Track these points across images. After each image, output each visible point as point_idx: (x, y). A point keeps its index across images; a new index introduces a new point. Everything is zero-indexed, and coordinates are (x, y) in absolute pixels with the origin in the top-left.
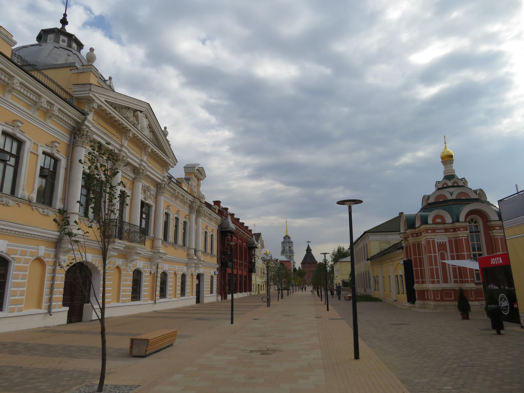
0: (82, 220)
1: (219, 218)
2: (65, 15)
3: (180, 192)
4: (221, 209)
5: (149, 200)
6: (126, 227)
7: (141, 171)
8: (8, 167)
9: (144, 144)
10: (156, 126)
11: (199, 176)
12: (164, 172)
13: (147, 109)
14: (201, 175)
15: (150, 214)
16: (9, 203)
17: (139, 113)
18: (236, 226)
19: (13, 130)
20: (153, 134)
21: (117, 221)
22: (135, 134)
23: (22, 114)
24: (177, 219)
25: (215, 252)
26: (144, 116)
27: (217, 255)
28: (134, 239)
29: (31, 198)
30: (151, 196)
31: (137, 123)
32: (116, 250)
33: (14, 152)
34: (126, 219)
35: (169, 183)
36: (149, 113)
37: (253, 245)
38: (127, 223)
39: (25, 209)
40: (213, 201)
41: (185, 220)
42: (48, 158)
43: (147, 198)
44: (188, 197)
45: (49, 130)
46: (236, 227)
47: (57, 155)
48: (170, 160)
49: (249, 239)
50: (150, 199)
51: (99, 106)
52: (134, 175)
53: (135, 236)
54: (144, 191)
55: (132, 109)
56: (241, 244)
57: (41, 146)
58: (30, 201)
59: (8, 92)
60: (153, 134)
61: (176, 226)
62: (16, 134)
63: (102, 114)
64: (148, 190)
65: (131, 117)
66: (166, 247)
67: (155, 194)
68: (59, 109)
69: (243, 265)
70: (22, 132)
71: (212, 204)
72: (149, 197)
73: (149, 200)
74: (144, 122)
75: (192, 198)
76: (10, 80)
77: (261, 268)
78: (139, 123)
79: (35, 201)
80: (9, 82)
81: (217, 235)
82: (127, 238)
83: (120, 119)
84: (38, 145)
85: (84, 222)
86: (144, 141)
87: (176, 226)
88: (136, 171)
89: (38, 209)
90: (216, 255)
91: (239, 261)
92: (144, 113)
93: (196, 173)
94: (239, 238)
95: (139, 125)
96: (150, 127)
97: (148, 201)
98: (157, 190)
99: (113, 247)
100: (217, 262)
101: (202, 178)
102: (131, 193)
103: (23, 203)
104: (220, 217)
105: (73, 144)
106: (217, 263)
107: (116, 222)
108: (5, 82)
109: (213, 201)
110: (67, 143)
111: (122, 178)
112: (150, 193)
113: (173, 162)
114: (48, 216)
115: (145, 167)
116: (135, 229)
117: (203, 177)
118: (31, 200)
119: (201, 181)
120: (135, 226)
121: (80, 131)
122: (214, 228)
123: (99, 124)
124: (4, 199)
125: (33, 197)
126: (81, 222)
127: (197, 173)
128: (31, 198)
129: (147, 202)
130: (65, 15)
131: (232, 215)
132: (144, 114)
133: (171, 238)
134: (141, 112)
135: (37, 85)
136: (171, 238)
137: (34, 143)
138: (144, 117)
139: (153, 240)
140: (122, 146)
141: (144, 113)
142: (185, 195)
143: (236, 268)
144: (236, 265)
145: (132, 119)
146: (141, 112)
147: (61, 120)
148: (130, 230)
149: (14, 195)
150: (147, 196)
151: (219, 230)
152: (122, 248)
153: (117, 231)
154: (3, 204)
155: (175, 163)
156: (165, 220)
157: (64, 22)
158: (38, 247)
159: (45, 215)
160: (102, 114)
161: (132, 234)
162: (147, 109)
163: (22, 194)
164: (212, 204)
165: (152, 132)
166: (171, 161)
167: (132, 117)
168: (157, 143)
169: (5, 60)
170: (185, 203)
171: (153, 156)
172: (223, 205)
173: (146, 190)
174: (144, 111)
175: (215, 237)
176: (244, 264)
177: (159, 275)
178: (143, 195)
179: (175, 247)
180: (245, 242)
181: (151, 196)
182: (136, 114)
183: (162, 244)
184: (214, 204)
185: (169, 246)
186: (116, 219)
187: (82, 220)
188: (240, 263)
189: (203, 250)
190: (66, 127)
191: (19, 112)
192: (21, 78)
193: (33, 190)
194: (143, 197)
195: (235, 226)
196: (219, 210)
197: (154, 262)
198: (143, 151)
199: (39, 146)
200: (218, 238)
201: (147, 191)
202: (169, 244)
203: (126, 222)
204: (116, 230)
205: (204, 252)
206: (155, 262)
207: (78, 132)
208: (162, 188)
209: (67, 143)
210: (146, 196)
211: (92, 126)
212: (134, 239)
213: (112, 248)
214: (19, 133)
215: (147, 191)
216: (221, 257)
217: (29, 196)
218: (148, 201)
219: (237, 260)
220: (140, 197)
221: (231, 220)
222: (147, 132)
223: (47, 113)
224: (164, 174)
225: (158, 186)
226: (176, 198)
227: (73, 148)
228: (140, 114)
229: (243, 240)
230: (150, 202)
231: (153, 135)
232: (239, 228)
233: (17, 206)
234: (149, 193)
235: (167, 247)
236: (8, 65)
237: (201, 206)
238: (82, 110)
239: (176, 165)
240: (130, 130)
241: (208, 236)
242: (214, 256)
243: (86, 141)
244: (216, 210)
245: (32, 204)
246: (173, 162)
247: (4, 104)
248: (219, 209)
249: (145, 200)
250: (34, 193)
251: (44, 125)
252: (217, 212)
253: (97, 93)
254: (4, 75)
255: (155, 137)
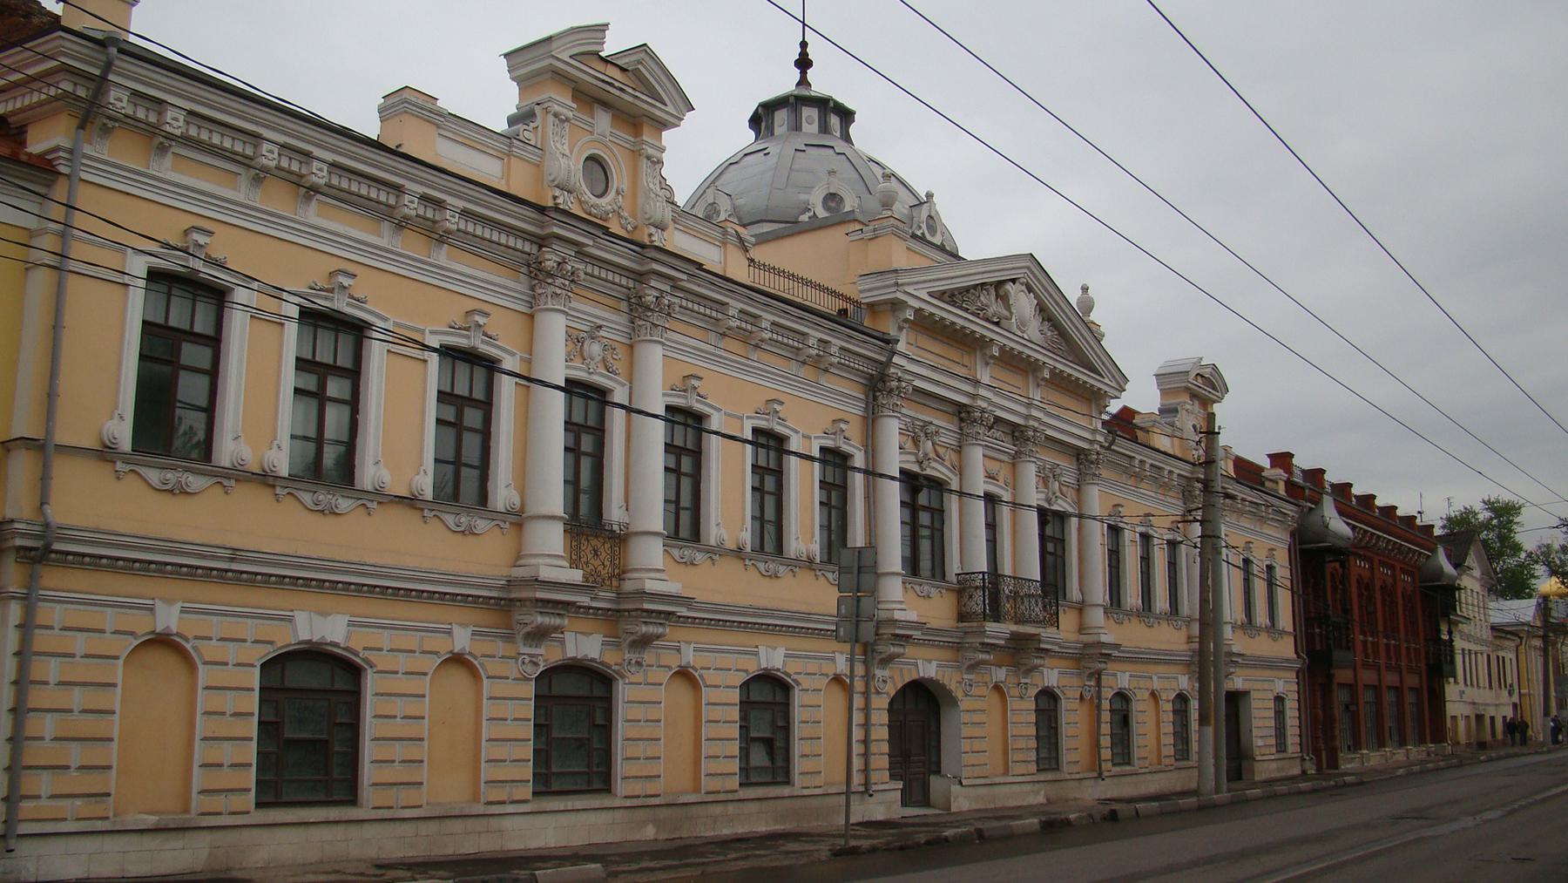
0: (747, 561)
1: (1289, 509)
2: (804, 45)
3: (1145, 459)
4: (1298, 479)
5: (1060, 501)
6: (1006, 590)
7: (1031, 433)
8: (467, 436)
9: (1093, 392)
10: (1058, 304)
11: (1207, 393)
12: (978, 367)
13: (1028, 268)
14: (1213, 389)
15: (1066, 537)
16: (337, 507)
17: (1009, 286)
18: (1350, 521)
19: (834, 440)
20: (1052, 326)
21: (984, 576)
22: (921, 310)
23: (355, 251)
24: (1146, 538)
25: (1285, 619)
26: (1024, 288)
27: (1295, 630)
28: (1030, 615)
29: (269, 466)
30: (1064, 489)
31: (1007, 314)
32: (989, 647)
33: (479, 394)
34: (1007, 568)
35: (1112, 443)
36: (1035, 276)
37: (1438, 581)
38: (1009, 577)
39: (805, 576)
40: (1269, 456)
41: (1268, 563)
42: (463, 370)
43: (1054, 499)
44: (1172, 469)
45: (199, 203)
46: (1354, 528)
47: (845, 448)
48: (1106, 381)
49: (1422, 560)
50: (1062, 499)
51: (918, 311)
52: (1014, 445)
53: (1032, 608)
54: (1044, 481)
55: (991, 284)
56: (1390, 581)
57: (815, 438)
58: (811, 561)
59: (304, 200)
60: (1052, 326)
61: (1146, 560)
62: (477, 346)
63: (926, 325)
64: (1054, 476)
65: (991, 303)
66: (1118, 623)
67: (1075, 482)
68: (740, 311)
69: (1404, 652)
70: (358, 301)
71: (1265, 463)
72: (1058, 494)
73: (1060, 501)
74: (1024, 304)
75: (1189, 467)
76: (306, 163)
77: (1489, 656)
78: (1011, 313)
79: (126, 444)
80: (304, 171)
81: (1287, 565)
82: (1013, 615)
83: (967, 324)
84: (811, 438)
85: (912, 587)
86: (934, 314)
87: (1146, 560)
88: (962, 413)
89: (296, 494)
90: (1291, 630)
91: (1361, 637)
92: (1021, 280)
93: (1194, 387)
94: (1380, 561)
95: (1013, 320)
96: (1042, 309)
97: (1058, 504)
98: (1079, 470)
99: (981, 641)
100: (1296, 652)
101: (1216, 398)
102: (1012, 493)
103: (236, 480)
104: (1296, 505)
105: (873, 413)
106: (1295, 656)
107: (984, 579)
108: (292, 173)
109: (1269, 456)
110: (861, 413)
111: (986, 459)
112: (1060, 483)
113: (1114, 384)
114: (335, 513)
115: (1038, 420)
116: (1030, 589)
117: (1219, 395)
118: (417, 495)
119: (1215, 405)
120: (1030, 580)
121: (884, 382)
122: (1273, 544)
123: (995, 378)
124: (463, 519)
125: (273, 462)
126: (906, 588)
127: (1196, 388)
128: (269, 466)
129: (1056, 507)
130: (804, 45)
131: (1343, 489)
132: (1022, 284)
133: (1132, 597)
134: (1014, 281)
135: (510, 207)
136: (1132, 597)
137: (803, 436)
138: (1023, 291)
139: (1081, 607)
140: (976, 383)
141: (1021, 280)
142: (1164, 466)
143: (1394, 668)
144: (1394, 659)
145: (995, 308)
146: (1014, 281)
147: (701, 316)
148: (1016, 593)
149: (210, 462)
150: (1054, 493)
151: (1295, 545)
152: (1003, 642)
153: (987, 602)
154: (171, 491)
155: (1118, 383)
156: (1110, 548)
157: (804, 63)
158: (756, 650)
159: (685, 563)
160: (926, 325)
161: (1023, 603)
162: (1028, 268)
163: (796, 548)
164: (1265, 463)
165: (1049, 320)
166: (1109, 383)
167: (993, 301)
168: (1063, 344)
169: (181, 81)
170: (1165, 487)
171: (1060, 382)
172: (1303, 461)
173: (916, 434)
174: (1022, 275)
175: (1282, 573)
176: (1365, 643)
177: (1106, 705)
178: (1042, 492)
179: (1146, 620)
180: (1403, 571)
181: (1064, 489)
182: (1001, 292)
183: (906, 588)
184: (1273, 466)
185: (1159, 622)
186: (983, 573)
187: (747, 561)
188: (1408, 649)
189: (1240, 616)
190: (861, 381)
191: (355, 251)
192: (176, 96)
193: (813, 537)
194: (1042, 496)
195: (1348, 524)
196: (1290, 485)
197: (1022, 664)
198: (1031, 378)
199: (427, 331)
200: (1291, 576)
201: (1051, 480)
202: (1129, 614)
203: (1006, 576)
204: (984, 598)
205: (1266, 627)
206: (1025, 665)
207: (880, 385)
208: (1028, 440)
209: (861, 413)
210: (1050, 493)
211: (1045, 414)
212: (1030, 615)
213: (980, 644)
214: (483, 341)
215: (1051, 480)
216: (1306, 633)
217: (807, 550)
218: (1058, 504)
219: (1395, 640)
220: (893, 460)
221: (1336, 507)
222: (1035, 329)
223: (818, 364)
224: (1094, 424)
225: (1082, 457)
226: (1139, 477)
227: (873, 421)
228: (1010, 289)
229: (1398, 566)
230: (943, 474)
231: (1051, 328)
232: (1370, 529)
233: (939, 595)
234: (1057, 484)
235: (1153, 626)
236: (278, 125)
237: (1195, 476)
238: (884, 333)
239: (1124, 390)
240: (992, 340)
241: (1127, 543)
242: (1283, 633)
243: (899, 403)
244: (1277, 483)
245: (814, 566)
246: (1114, 384)
247: (281, 228)
248: (1288, 479)
249: (1050, 504)
250: (422, 472)
251: (269, 218)
252: (1282, 491)
253: (909, 284)
254: (219, 133)
255: (1056, 333)
